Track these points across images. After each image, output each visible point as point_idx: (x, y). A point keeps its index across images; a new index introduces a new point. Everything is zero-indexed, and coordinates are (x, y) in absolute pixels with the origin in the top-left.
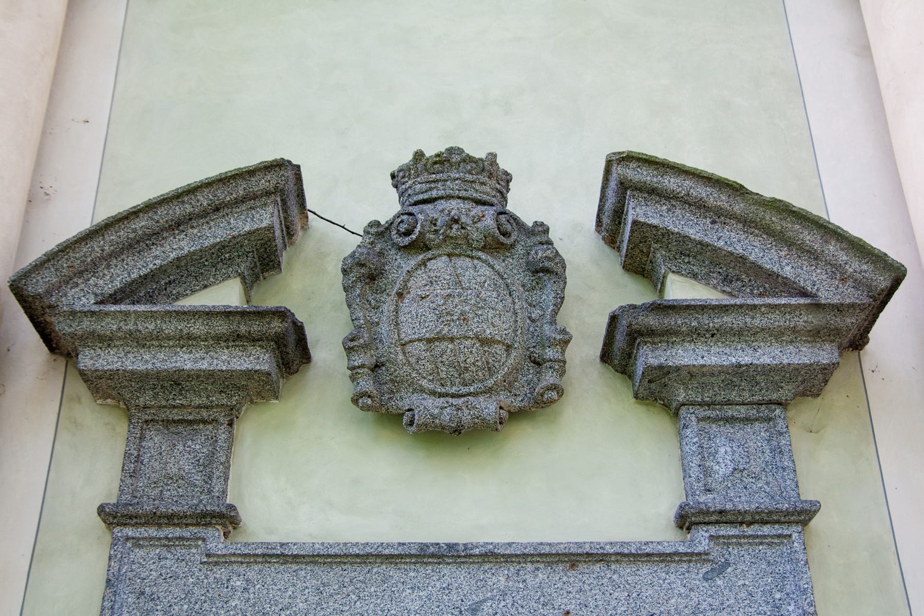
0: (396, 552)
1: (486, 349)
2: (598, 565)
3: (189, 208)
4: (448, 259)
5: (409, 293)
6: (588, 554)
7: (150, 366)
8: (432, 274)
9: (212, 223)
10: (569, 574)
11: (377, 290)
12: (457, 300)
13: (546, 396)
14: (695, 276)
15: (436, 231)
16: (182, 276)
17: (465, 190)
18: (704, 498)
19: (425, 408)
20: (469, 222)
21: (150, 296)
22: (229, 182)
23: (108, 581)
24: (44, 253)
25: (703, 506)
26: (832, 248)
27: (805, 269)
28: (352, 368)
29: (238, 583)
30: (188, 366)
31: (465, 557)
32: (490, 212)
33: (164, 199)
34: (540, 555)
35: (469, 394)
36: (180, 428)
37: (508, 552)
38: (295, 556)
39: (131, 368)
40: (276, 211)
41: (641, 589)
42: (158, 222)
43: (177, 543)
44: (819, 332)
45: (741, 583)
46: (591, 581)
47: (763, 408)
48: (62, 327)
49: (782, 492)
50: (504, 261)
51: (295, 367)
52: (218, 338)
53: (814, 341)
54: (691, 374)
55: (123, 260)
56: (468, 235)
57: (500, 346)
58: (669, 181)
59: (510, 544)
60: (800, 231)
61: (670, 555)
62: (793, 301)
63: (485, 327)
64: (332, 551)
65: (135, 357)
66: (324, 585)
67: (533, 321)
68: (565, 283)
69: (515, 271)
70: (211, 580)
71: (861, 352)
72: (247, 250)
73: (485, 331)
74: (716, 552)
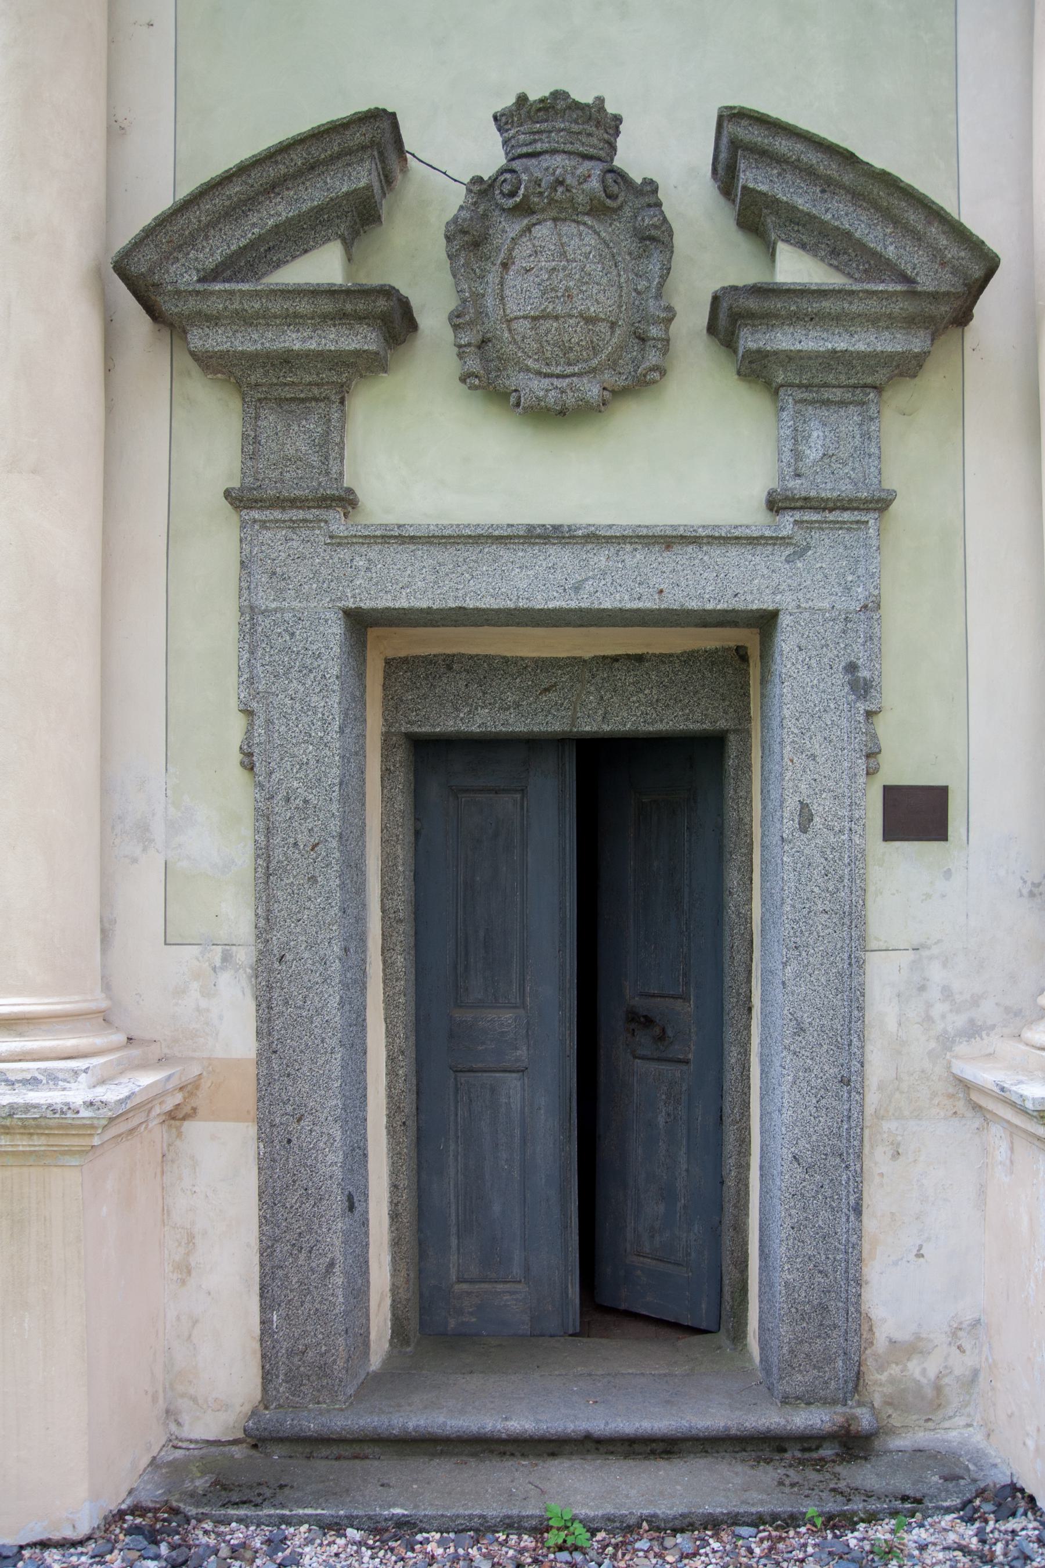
0: (506, 534)
1: (590, 327)
2: (691, 547)
3: (283, 169)
4: (553, 225)
5: (513, 263)
6: (682, 537)
7: (259, 347)
8: (537, 244)
9: (308, 184)
10: (664, 555)
11: (482, 258)
12: (561, 275)
13: (648, 377)
14: (803, 246)
15: (541, 194)
16: (281, 242)
17: (572, 143)
18: (793, 483)
19: (530, 390)
20: (575, 183)
21: (251, 266)
22: (322, 136)
23: (242, 563)
24: (141, 228)
25: (789, 493)
26: (826, 304)
27: (908, 249)
28: (460, 346)
29: (361, 563)
30: (297, 346)
31: (569, 538)
32: (596, 169)
33: (257, 161)
34: (638, 537)
35: (573, 375)
36: (293, 406)
37: (608, 534)
38: (412, 537)
39: (240, 348)
40: (374, 165)
41: (728, 570)
42: (252, 186)
43: (301, 525)
44: (914, 319)
45: (818, 565)
46: (684, 561)
47: (858, 391)
48: (169, 307)
49: (865, 479)
50: (611, 225)
51: (402, 338)
52: (325, 317)
53: (909, 327)
54: (790, 358)
55: (221, 230)
56: (573, 199)
57: (605, 324)
58: (780, 143)
59: (610, 526)
60: (906, 209)
61: (756, 538)
62: (891, 287)
63: (589, 304)
64: (446, 533)
65: (243, 337)
66: (440, 564)
67: (639, 293)
68: (672, 252)
69: (622, 237)
70: (336, 560)
71: (966, 328)
72: (346, 210)
73: (589, 309)
74: (799, 536)
